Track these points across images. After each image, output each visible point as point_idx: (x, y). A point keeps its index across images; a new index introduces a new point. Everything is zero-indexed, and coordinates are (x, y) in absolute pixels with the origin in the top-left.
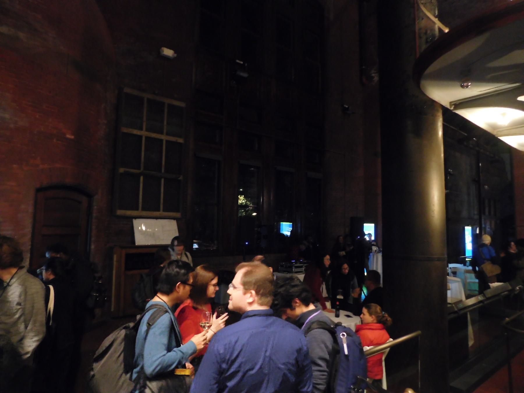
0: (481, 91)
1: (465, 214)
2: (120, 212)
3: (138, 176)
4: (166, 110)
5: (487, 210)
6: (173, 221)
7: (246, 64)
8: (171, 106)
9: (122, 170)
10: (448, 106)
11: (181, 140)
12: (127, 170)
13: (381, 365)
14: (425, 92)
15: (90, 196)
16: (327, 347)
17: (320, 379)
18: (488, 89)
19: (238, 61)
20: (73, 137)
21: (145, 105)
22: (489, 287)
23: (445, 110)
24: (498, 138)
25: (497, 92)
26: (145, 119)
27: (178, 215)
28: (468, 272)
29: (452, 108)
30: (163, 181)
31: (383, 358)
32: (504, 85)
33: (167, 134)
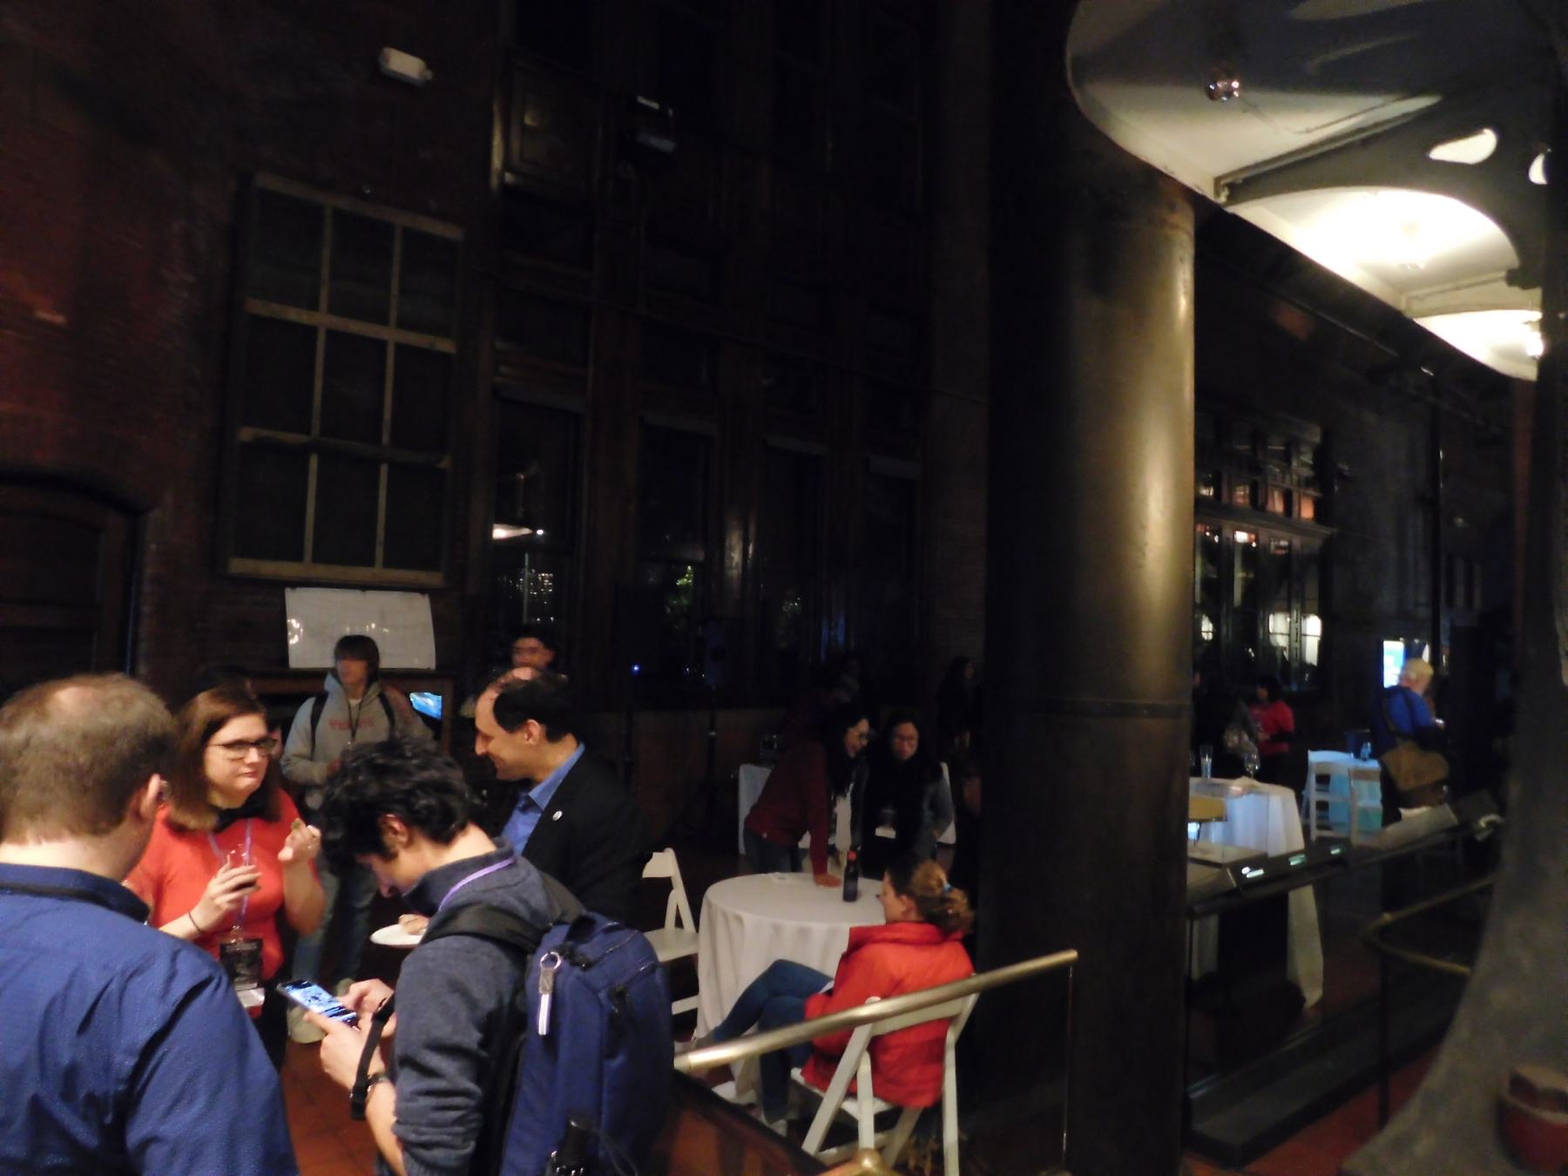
0: (1308, 131)
1: (1386, 600)
2: (239, 566)
3: (303, 453)
4: (397, 248)
5: (1460, 590)
6: (418, 596)
7: (671, 112)
8: (411, 236)
9: (246, 434)
10: (1208, 191)
11: (445, 346)
12: (266, 433)
13: (940, 1058)
14: (1100, 126)
15: (133, 512)
16: (472, 1004)
17: (433, 1124)
18: (1336, 118)
19: (642, 100)
20: (60, 319)
21: (328, 231)
22: (1398, 817)
23: (1195, 199)
24: (1414, 323)
25: (1363, 135)
26: (325, 272)
27: (434, 579)
28: (1360, 775)
29: (1222, 199)
30: (384, 469)
31: (951, 1037)
32: (1383, 106)
33: (402, 324)
